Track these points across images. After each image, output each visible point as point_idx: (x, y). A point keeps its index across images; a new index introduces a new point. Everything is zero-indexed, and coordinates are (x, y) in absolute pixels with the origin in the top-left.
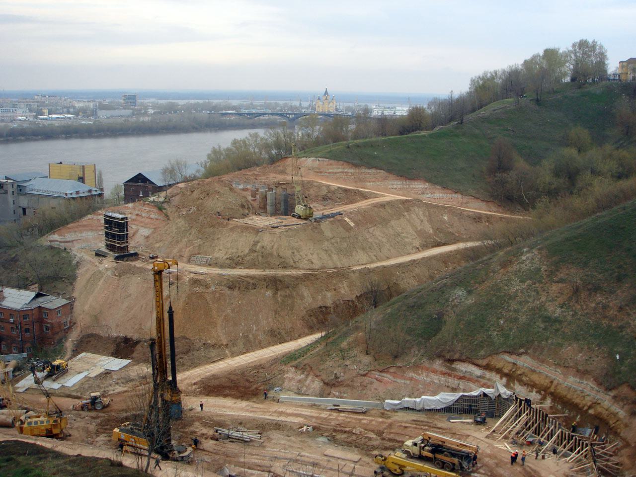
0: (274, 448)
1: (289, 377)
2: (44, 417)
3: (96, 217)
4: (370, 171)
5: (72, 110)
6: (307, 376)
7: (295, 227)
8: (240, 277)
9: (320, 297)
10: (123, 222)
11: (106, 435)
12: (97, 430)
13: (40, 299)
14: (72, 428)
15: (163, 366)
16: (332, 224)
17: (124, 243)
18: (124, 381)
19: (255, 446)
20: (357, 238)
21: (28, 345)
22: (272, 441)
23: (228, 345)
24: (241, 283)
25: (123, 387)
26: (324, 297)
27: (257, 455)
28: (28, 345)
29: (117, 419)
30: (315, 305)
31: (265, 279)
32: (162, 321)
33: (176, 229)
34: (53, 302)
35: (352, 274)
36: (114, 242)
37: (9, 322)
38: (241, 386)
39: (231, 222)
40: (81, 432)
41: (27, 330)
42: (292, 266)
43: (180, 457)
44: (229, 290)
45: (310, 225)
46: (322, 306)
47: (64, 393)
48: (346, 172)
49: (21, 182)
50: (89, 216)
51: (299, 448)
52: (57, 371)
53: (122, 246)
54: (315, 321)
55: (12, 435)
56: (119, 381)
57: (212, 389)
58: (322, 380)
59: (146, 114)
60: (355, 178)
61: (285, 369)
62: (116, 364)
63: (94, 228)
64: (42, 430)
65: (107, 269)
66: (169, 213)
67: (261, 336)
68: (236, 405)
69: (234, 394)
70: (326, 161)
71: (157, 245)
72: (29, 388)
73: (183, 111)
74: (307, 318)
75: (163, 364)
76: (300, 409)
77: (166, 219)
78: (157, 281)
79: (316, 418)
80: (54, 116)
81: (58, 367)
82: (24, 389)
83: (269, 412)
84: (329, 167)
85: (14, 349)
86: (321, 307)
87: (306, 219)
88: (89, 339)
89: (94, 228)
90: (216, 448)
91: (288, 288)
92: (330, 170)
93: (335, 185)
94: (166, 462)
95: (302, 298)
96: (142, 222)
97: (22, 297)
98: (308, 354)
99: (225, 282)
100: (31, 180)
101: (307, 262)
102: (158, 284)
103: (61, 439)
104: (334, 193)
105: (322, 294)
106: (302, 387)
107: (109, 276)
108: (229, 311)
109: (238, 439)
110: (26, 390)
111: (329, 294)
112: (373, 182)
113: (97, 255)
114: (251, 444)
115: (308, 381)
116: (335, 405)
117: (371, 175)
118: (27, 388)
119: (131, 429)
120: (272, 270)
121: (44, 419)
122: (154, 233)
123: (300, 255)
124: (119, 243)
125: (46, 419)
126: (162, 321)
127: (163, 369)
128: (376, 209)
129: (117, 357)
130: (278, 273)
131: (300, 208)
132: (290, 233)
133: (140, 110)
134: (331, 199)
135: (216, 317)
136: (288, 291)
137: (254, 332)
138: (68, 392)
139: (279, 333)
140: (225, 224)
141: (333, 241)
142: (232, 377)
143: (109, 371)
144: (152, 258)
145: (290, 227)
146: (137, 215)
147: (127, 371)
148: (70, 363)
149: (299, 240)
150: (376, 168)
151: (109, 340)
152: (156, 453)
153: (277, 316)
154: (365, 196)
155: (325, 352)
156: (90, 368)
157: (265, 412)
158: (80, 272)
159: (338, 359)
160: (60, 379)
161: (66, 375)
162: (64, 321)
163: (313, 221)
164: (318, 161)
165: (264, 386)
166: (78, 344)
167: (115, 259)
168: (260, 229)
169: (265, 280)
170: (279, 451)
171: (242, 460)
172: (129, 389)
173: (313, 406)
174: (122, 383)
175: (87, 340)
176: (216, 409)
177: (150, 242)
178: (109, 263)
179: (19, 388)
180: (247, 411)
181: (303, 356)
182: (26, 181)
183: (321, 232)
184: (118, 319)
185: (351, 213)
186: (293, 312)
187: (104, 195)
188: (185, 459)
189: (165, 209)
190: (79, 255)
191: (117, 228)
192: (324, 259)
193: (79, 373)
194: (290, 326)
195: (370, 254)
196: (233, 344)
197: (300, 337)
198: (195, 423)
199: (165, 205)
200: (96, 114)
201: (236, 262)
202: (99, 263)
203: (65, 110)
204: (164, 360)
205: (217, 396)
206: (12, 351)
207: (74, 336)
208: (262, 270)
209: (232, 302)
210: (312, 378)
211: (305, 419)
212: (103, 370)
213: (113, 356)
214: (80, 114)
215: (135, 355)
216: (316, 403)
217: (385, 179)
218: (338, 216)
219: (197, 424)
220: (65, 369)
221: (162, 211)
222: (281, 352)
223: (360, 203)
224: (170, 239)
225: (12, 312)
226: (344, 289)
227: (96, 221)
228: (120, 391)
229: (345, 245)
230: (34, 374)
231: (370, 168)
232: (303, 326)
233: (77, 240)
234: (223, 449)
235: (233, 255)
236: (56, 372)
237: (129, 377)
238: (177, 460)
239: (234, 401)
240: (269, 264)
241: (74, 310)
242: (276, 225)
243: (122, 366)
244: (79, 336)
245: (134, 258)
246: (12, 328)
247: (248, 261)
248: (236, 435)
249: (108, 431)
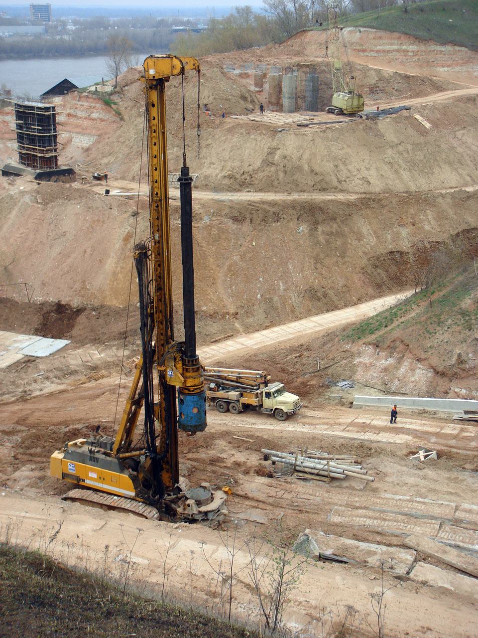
0: (396, 493)
1: (365, 364)
4: (443, 48)
6: (400, 361)
8: (251, 203)
9: (389, 236)
11: (33, 467)
12: (15, 458)
18: (58, 373)
19: (353, 489)
20: (439, 146)
26: (397, 237)
27: (366, 508)
29: (55, 435)
30: (382, 250)
31: (293, 205)
33: (135, 134)
35: (440, 200)
39: (227, 120)
42: (336, 188)
43: (200, 512)
44: (233, 223)
46: (394, 250)
48: (404, 51)
51: (451, 493)
53: (48, 155)
54: (384, 275)
56: (51, 375)
58: (432, 367)
59: (65, 31)
60: (419, 59)
61: (355, 349)
65: (23, 193)
66: (122, 110)
67: (294, 299)
71: (105, 161)
73: (116, 28)
74: (370, 269)
75: (166, 304)
77: (118, 119)
78: (153, 105)
79: (437, 435)
83: (340, 424)
84: (376, 42)
86: (392, 253)
87: (351, 115)
92: (379, 48)
93: (388, 70)
94: (176, 525)
95: (360, 237)
96: (77, 126)
98: (397, 323)
99: (227, 211)
102: (154, 112)
104: (388, 81)
105: (393, 231)
106: (391, 381)
107: (28, 203)
108: (236, 258)
109: (318, 475)
111: (404, 232)
112: (449, 66)
114: (345, 484)
115: (402, 370)
116: (466, 412)
117: (444, 55)
119: (91, 451)
120: (302, 193)
122: (98, 142)
124: (42, 151)
127: (166, 317)
128: (462, 105)
129: (44, 336)
130: (314, 197)
131: (341, 96)
132: (330, 134)
133: (56, 27)
135: (214, 267)
139: (325, 295)
140: (217, 122)
141: (401, 148)
143: (31, 358)
144: (98, 178)
146: (69, 115)
147: (64, 357)
150: (454, 43)
152: (147, 504)
153: (319, 266)
154: (439, 88)
155: (430, 318)
157: (331, 425)
159: (458, 329)
163: (364, 117)
164: (358, 33)
165: (316, 379)
167: (36, 178)
168: (279, 127)
169: (294, 207)
170: (409, 501)
171: (336, 519)
172: (70, 388)
174: (56, 377)
177: (92, 156)
178: (26, 184)
181: (386, 326)
183: (379, 135)
184: (45, 274)
185: (424, 108)
186: (346, 259)
188: (210, 516)
189: (115, 104)
191: (38, 126)
192: (387, 178)
194: (342, 282)
195: (460, 171)
197: (360, 301)
199: (115, 98)
201: (240, 183)
202: (9, 184)
204: (167, 296)
209: (239, 243)
210: (411, 363)
211: (414, 438)
213: (37, 335)
215: (75, 332)
216: (427, 409)
218: (404, 111)
219: (221, 443)
221: (110, 106)
222: (333, 325)
223: (432, 96)
224: (126, 150)
228: (53, 390)
229: (420, 156)
231: (444, 44)
234: (286, 496)
237: (68, 366)
238: (192, 521)
242: (304, 122)
243: (55, 350)
245: (67, 177)
247: (261, 180)
248: (312, 465)
249: (38, 459)
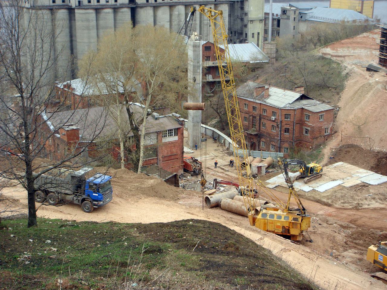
2: (283, 211)
3: (371, 36)
13: (304, 102)
18: (382, 197)
25: (380, 203)
28: (286, 145)
29: (372, 235)
40: (325, 239)
41: (287, 130)
49: (303, 10)
50: (365, 34)
52: (310, 173)
56: (377, 197)
63: (367, 46)
65: (377, 83)
81: (312, 170)
82: (274, 186)
85: (272, 147)
89: (367, 46)
97: (286, 97)
100: (312, 8)
113: (369, 69)
118: (277, 185)
121: (282, 213)
125: (285, 214)
129: (376, 172)
138: (318, 197)
143: (365, 184)
148: (325, 169)
156: (346, 178)
158: (349, 83)
160: (312, 182)
162: (325, 127)
174: (379, 199)
179: (269, 183)
182: (308, 9)
187: (380, 36)
190: (349, 67)
202: (370, 76)
206: (269, 148)
207: (333, 144)
213: (372, 170)
225: (275, 110)
227: (371, 40)
230: (287, 173)
233: (349, 56)
241: (337, 119)
243: (382, 182)
244: (339, 144)
249: (360, 247)
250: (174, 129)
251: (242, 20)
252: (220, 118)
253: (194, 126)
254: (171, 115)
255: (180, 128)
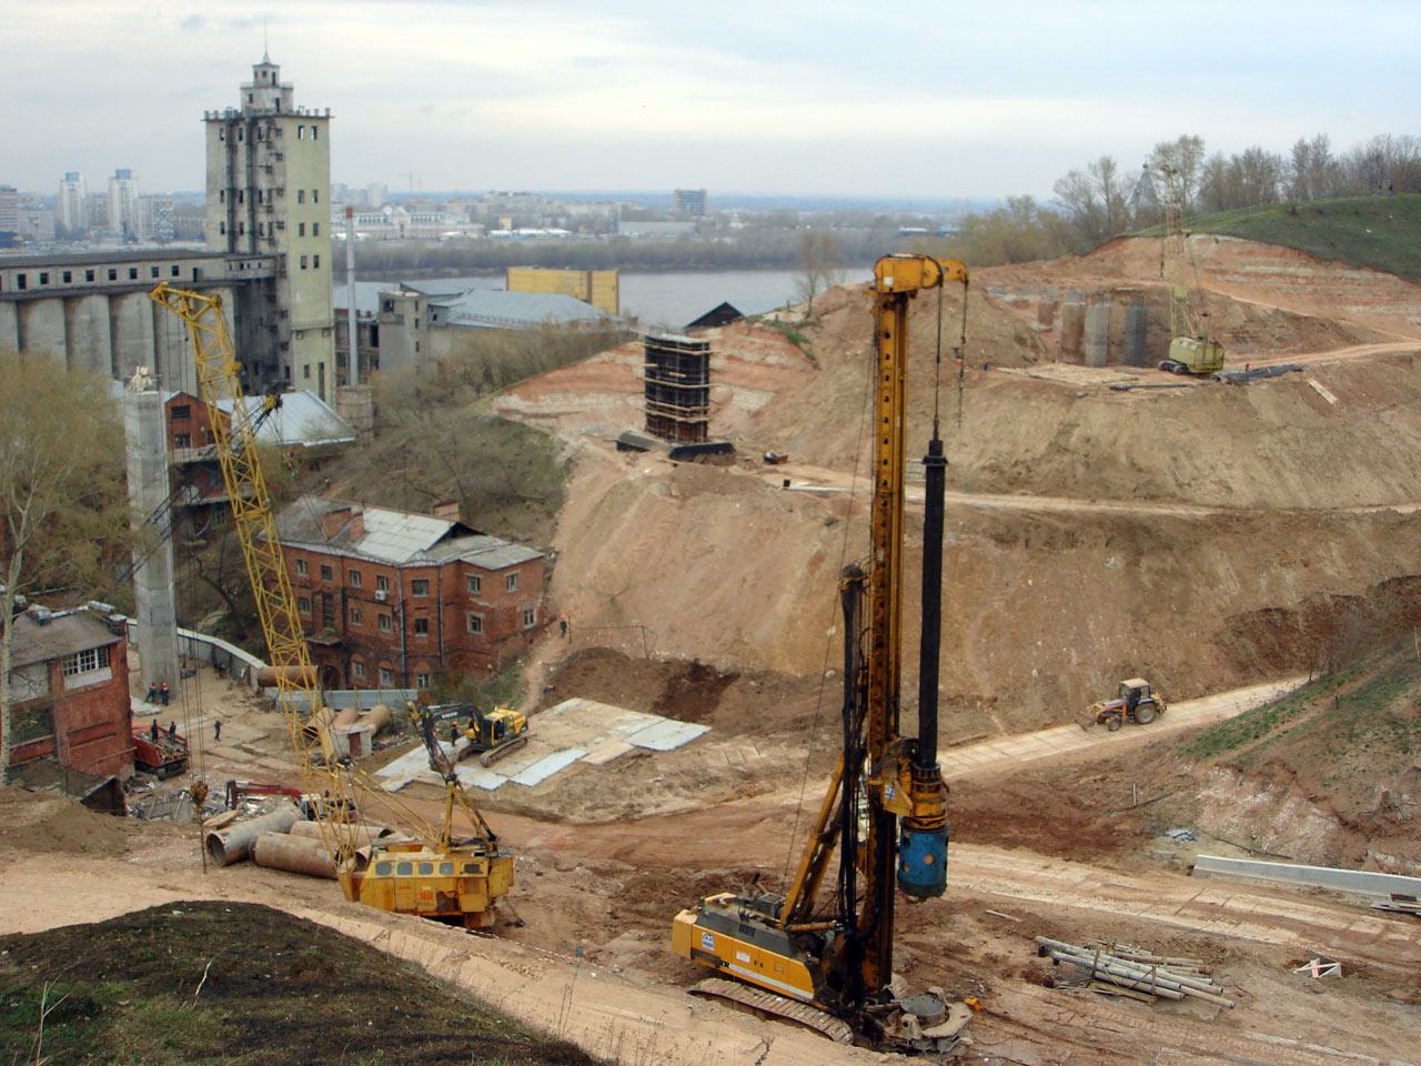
1: (1217, 801)
2: (435, 850)
3: (620, 359)
4: (1355, 275)
5: (562, 221)
6: (1279, 799)
7: (1178, 392)
8: (1027, 514)
9: (1263, 583)
10: (696, 353)
12: (613, 915)
13: (463, 543)
14: (526, 899)
15: (889, 677)
16: (1280, 391)
17: (698, 412)
18: (687, 780)
19: (1196, 1019)
20: (1350, 434)
21: (423, 667)
22: (1256, 1006)
23: (996, 700)
24: (1031, 528)
25: (687, 798)
26: (1275, 585)
28: (423, 667)
29: (680, 884)
30: (1251, 605)
31: (1100, 521)
32: (895, 498)
34: (492, 552)
35: (1353, 525)
36: (672, 411)
37: (374, 601)
38: (1056, 819)
39: (991, 374)
40: (557, 915)
42: (1173, 496)
43: (924, 1038)
45: (1218, 390)
46: (1271, 606)
47: (511, 803)
48: (1291, 275)
50: (605, 356)
52: (496, 738)
54: (1253, 649)
55: (307, 899)
56: (676, 782)
57: (962, 821)
58: (1336, 814)
60: (1315, 291)
61: (1200, 773)
62: (666, 734)
64: (426, 896)
65: (648, 479)
66: (818, 353)
68: (1049, 874)
69: (1038, 841)
70: (1235, 244)
71: (784, 433)
72: (413, 781)
74: (1228, 638)
75: (889, 672)
76: (1274, 901)
77: (811, 367)
79: (1343, 934)
80: (524, 231)
81: (500, 727)
82: (400, 784)
84: (1243, 259)
85: (385, 676)
86: (1267, 610)
87: (1202, 375)
88: (590, 662)
90: (1053, 1013)
91: (1171, 549)
92: (1248, 268)
93: (1264, 306)
95: (1212, 581)
96: (743, 376)
97: (414, 533)
99: (985, 524)
101: (1214, 487)
102: (889, 347)
103: (487, 931)
104: (1263, 323)
105: (1271, 574)
106: (1263, 833)
107: (654, 496)
108: (998, 605)
109: (1133, 989)
110: (406, 786)
111: (1289, 577)
112: (1366, 304)
113: (623, 446)
114: (1182, 1009)
116: (1395, 897)
119: (742, 916)
120: (1115, 502)
122: (774, 402)
123: (1196, 468)
124: (683, 414)
125: (441, 856)
126: (895, 498)
128: (1389, 368)
129: (669, 716)
131: (1185, 344)
132: (1165, 405)
133: (713, 224)
134: (1256, 339)
136: (1170, 560)
137: (1073, 667)
138: (522, 801)
141: (1285, 434)
142: (1023, 791)
145: (1163, 391)
146: (730, 358)
147: (699, 754)
148: (534, 721)
149: (1190, 426)
150: (1376, 268)
151: (648, 667)
152: (832, 1015)
154: (1349, 338)
155: (1336, 727)
156: (591, 739)
157: (1155, 903)
158: (575, 485)
159: (1386, 748)
161: (521, 751)
162: (525, 609)
163: (1224, 380)
164: (1214, 244)
166: (560, 673)
167: (671, 456)
168: (1080, 390)
169: (1100, 525)
170: (1297, 1048)
172: (705, 806)
173: (1316, 894)
175: (584, 664)
176: (985, 882)
177: (763, 425)
178: (654, 465)
180: (1092, 893)
181: (1257, 737)
185: (1325, 369)
186: (1187, 617)
188: (942, 1046)
190: (573, 443)
191: (681, 372)
193: (559, 751)
194: (1178, 657)
195: (1387, 479)
196: (1012, 698)
197: (1209, 690)
198: (957, 917)
199: (807, 333)
200: (616, 230)
202: (628, 464)
203: (548, 220)
205: (982, 842)
206: (377, 680)
207: (548, 654)
208: (1087, 501)
210: (1299, 804)
211: (1302, 935)
212: (630, 747)
213: (657, 713)
214: (581, 228)
215: (720, 712)
216: (1325, 886)
217: (1398, 298)
220: (516, 736)
224: (820, 418)
225: (384, 572)
226: (1333, 562)
229: (1318, 449)
232: (1218, 659)
233: (569, 413)
234: (1076, 1022)
235: (1001, 459)
236: (494, 742)
239: (1042, 861)
240: (1107, 488)
241: (554, 584)
245: (721, 457)
246: (381, 616)
248: (1125, 971)
249: (651, 921)
250: (99, 649)
251: (274, 329)
252: (231, 605)
253: (156, 634)
254: (86, 608)
255: (115, 644)
